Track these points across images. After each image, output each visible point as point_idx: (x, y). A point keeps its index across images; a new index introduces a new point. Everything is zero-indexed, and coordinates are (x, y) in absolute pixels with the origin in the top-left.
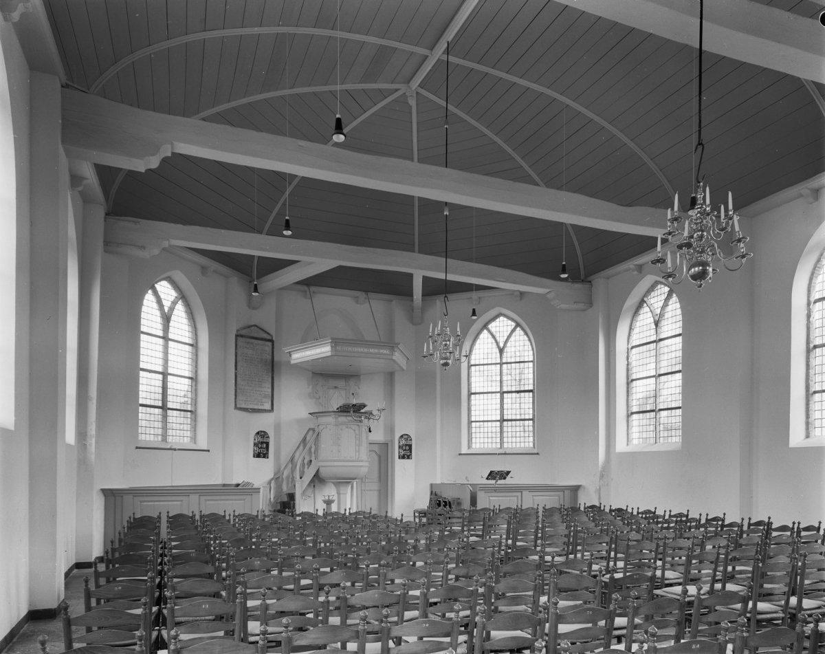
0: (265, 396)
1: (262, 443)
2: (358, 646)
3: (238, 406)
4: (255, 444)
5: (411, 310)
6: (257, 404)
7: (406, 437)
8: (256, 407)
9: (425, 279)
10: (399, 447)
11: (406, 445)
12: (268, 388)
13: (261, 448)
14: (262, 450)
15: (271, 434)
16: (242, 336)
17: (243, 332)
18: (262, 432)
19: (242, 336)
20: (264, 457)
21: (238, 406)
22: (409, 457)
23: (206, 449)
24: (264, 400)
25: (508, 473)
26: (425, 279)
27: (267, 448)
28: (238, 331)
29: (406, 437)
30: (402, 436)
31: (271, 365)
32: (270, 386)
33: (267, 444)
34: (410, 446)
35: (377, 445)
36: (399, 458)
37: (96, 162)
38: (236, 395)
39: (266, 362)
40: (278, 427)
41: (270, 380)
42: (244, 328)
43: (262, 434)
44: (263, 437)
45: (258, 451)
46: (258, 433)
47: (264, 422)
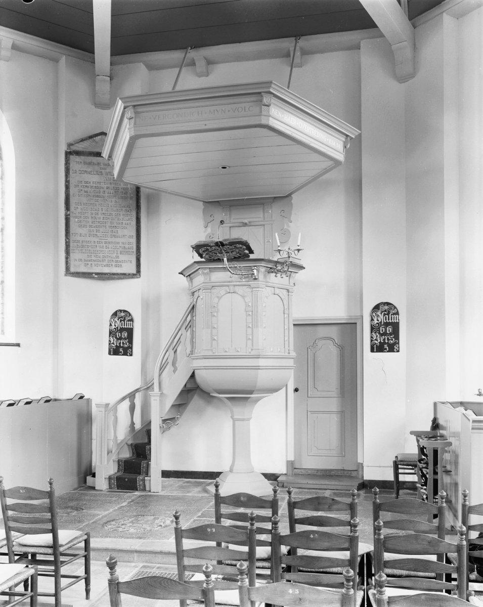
0: (125, 251)
1: (122, 330)
2: (350, 553)
3: (72, 270)
4: (110, 333)
5: (388, 54)
6: (107, 266)
7: (386, 307)
8: (106, 270)
9: (442, 592)
10: (373, 329)
11: (387, 324)
12: (131, 237)
13: (121, 338)
14: (122, 341)
15: (137, 315)
16: (78, 153)
17: (80, 147)
18: (121, 311)
19: (78, 153)
20: (125, 354)
21: (72, 270)
22: (392, 348)
23: (14, 342)
24: (122, 257)
25: (25, 404)
26: (442, 592)
27: (130, 338)
28: (70, 145)
29: (386, 308)
30: (377, 308)
31: (134, 199)
32: (134, 233)
33: (130, 332)
34: (396, 326)
35: (334, 328)
36: (372, 351)
37: (304, 270)
38: (67, 252)
39: (126, 193)
40: (148, 305)
41: (134, 222)
42: (82, 140)
43: (122, 315)
44: (122, 319)
45: (116, 343)
46: (115, 314)
47: (124, 295)
